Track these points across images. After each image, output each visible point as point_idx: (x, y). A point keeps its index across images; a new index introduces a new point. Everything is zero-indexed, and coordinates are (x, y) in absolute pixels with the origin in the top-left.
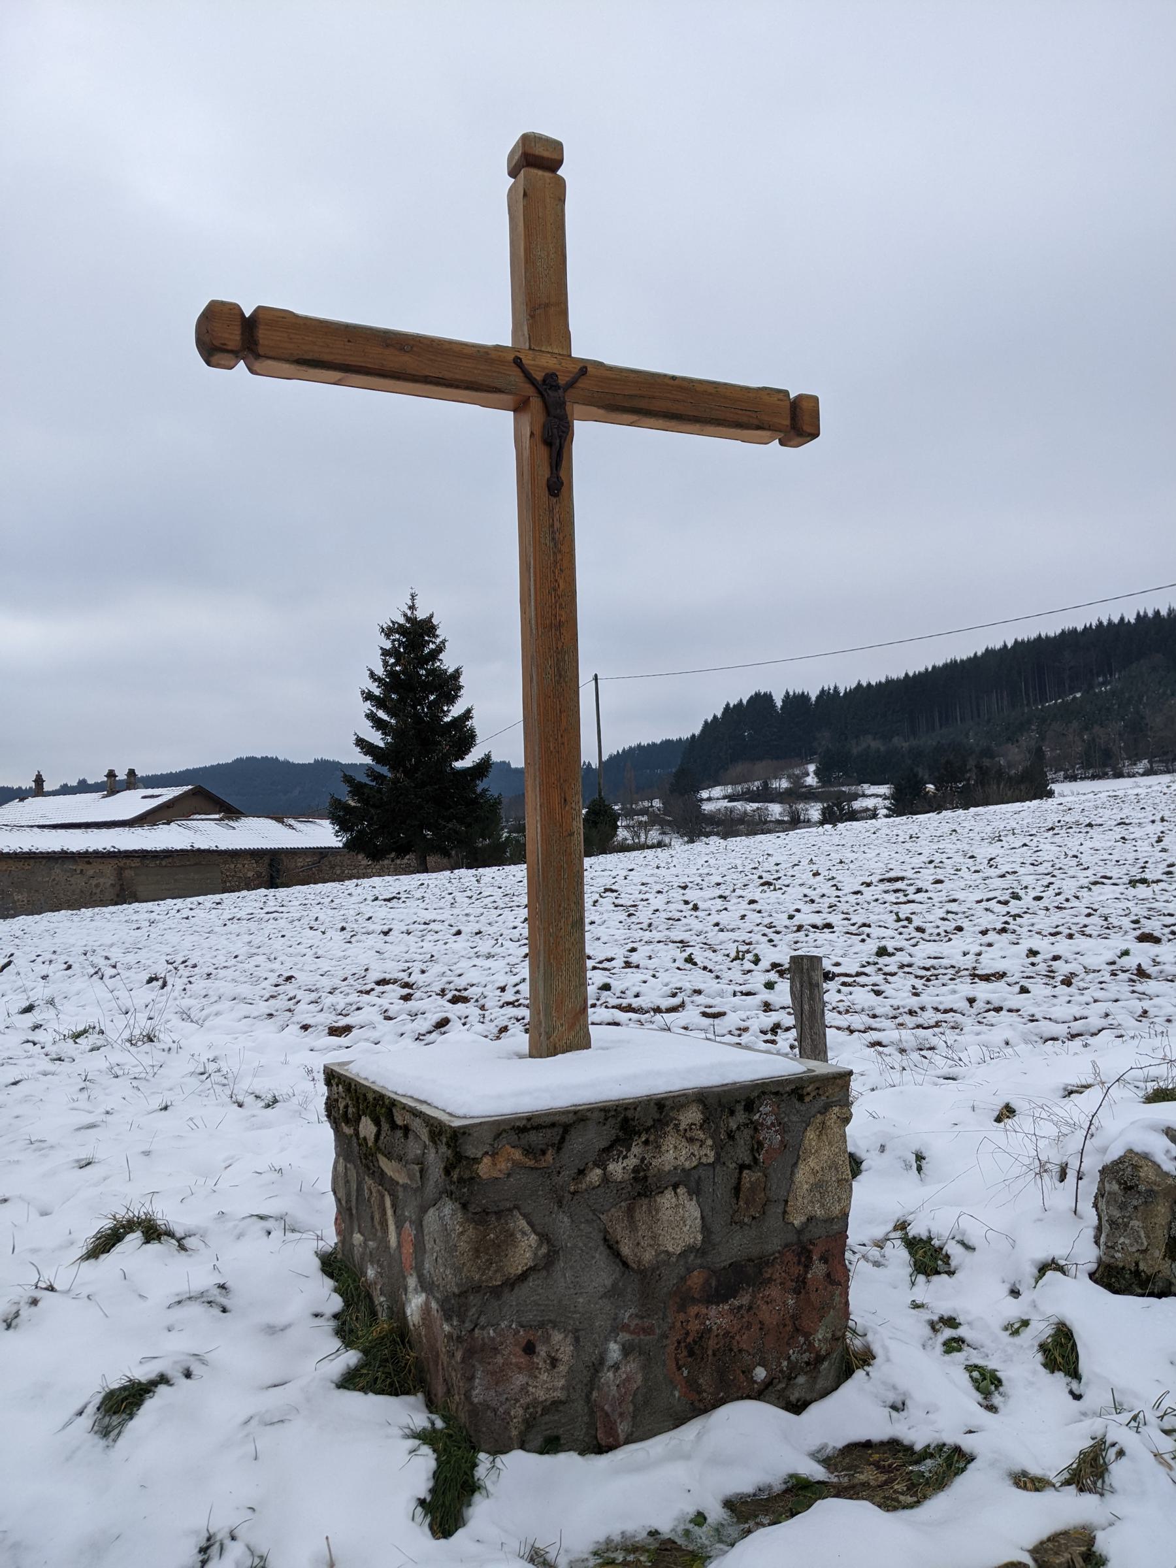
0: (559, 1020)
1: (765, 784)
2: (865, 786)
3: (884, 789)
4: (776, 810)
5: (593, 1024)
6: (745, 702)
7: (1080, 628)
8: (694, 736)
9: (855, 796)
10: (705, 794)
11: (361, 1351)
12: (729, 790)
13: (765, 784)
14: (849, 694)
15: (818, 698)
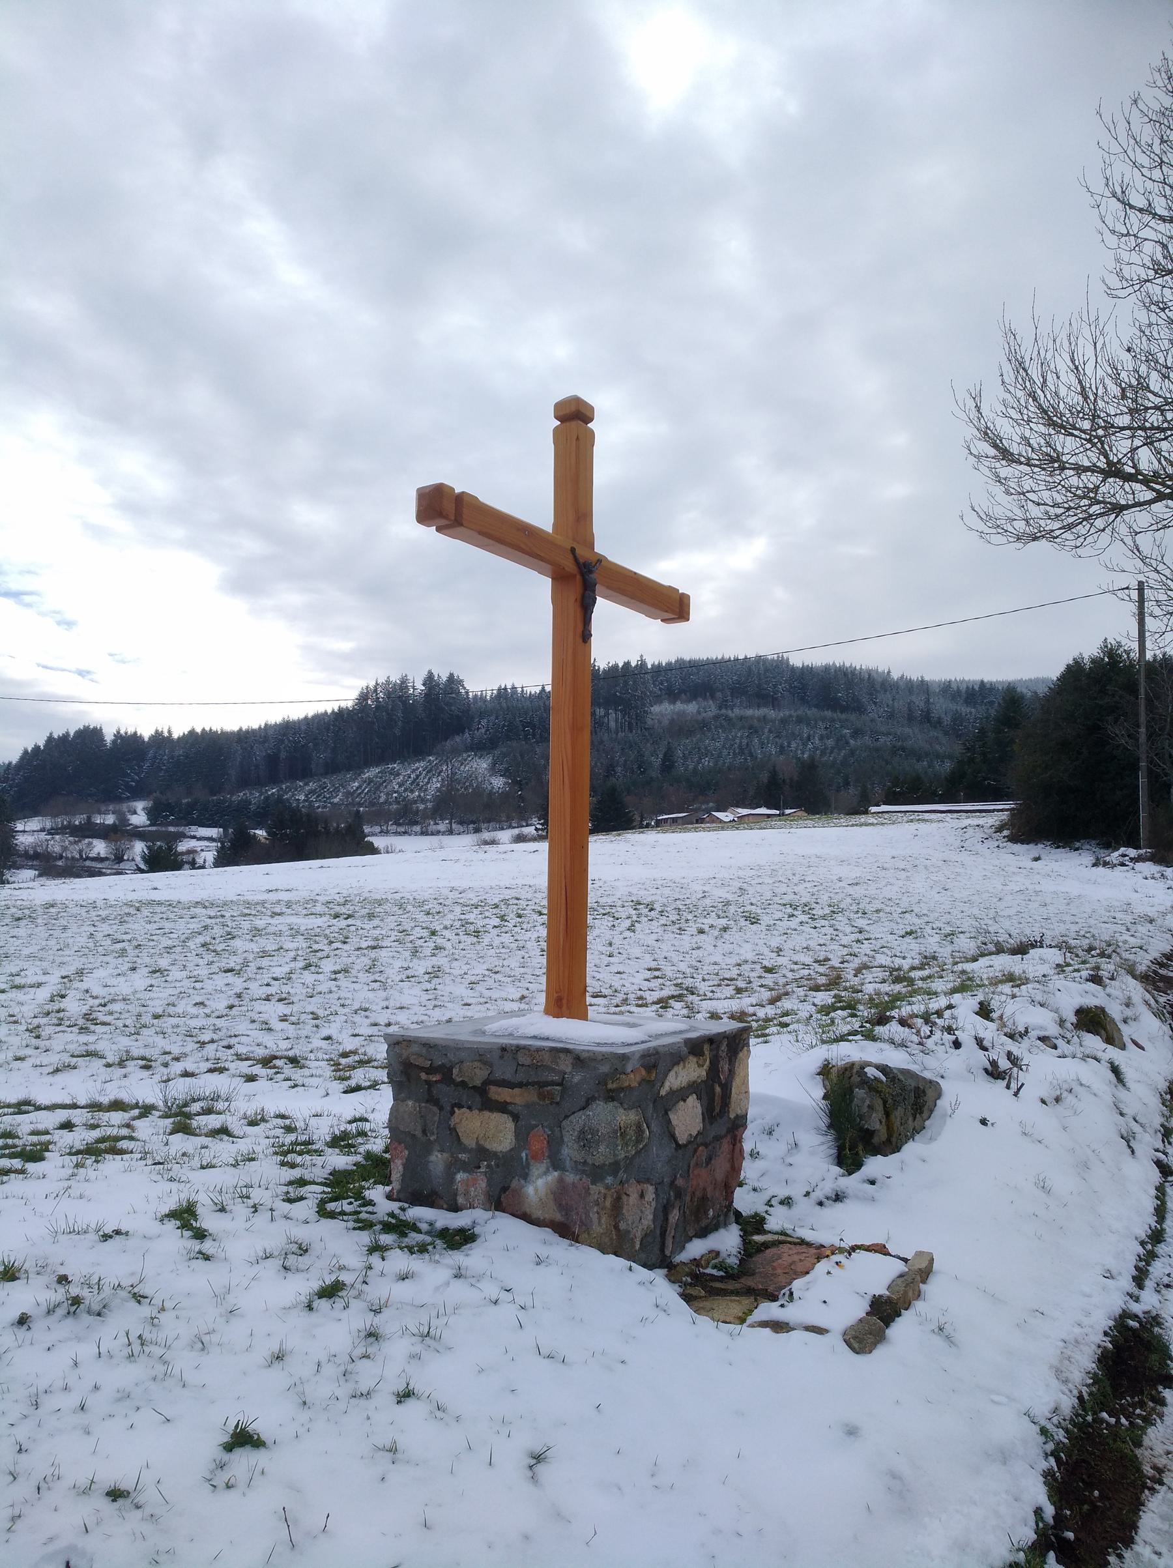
0: (567, 996)
1: (89, 818)
2: (193, 827)
3: (213, 832)
4: (100, 847)
5: (567, 996)
6: (72, 734)
7: (41, 744)
8: (10, 763)
9: (182, 836)
10: (20, 826)
11: (659, 1267)
12: (48, 824)
13: (89, 818)
14: (183, 739)
15: (114, 742)
